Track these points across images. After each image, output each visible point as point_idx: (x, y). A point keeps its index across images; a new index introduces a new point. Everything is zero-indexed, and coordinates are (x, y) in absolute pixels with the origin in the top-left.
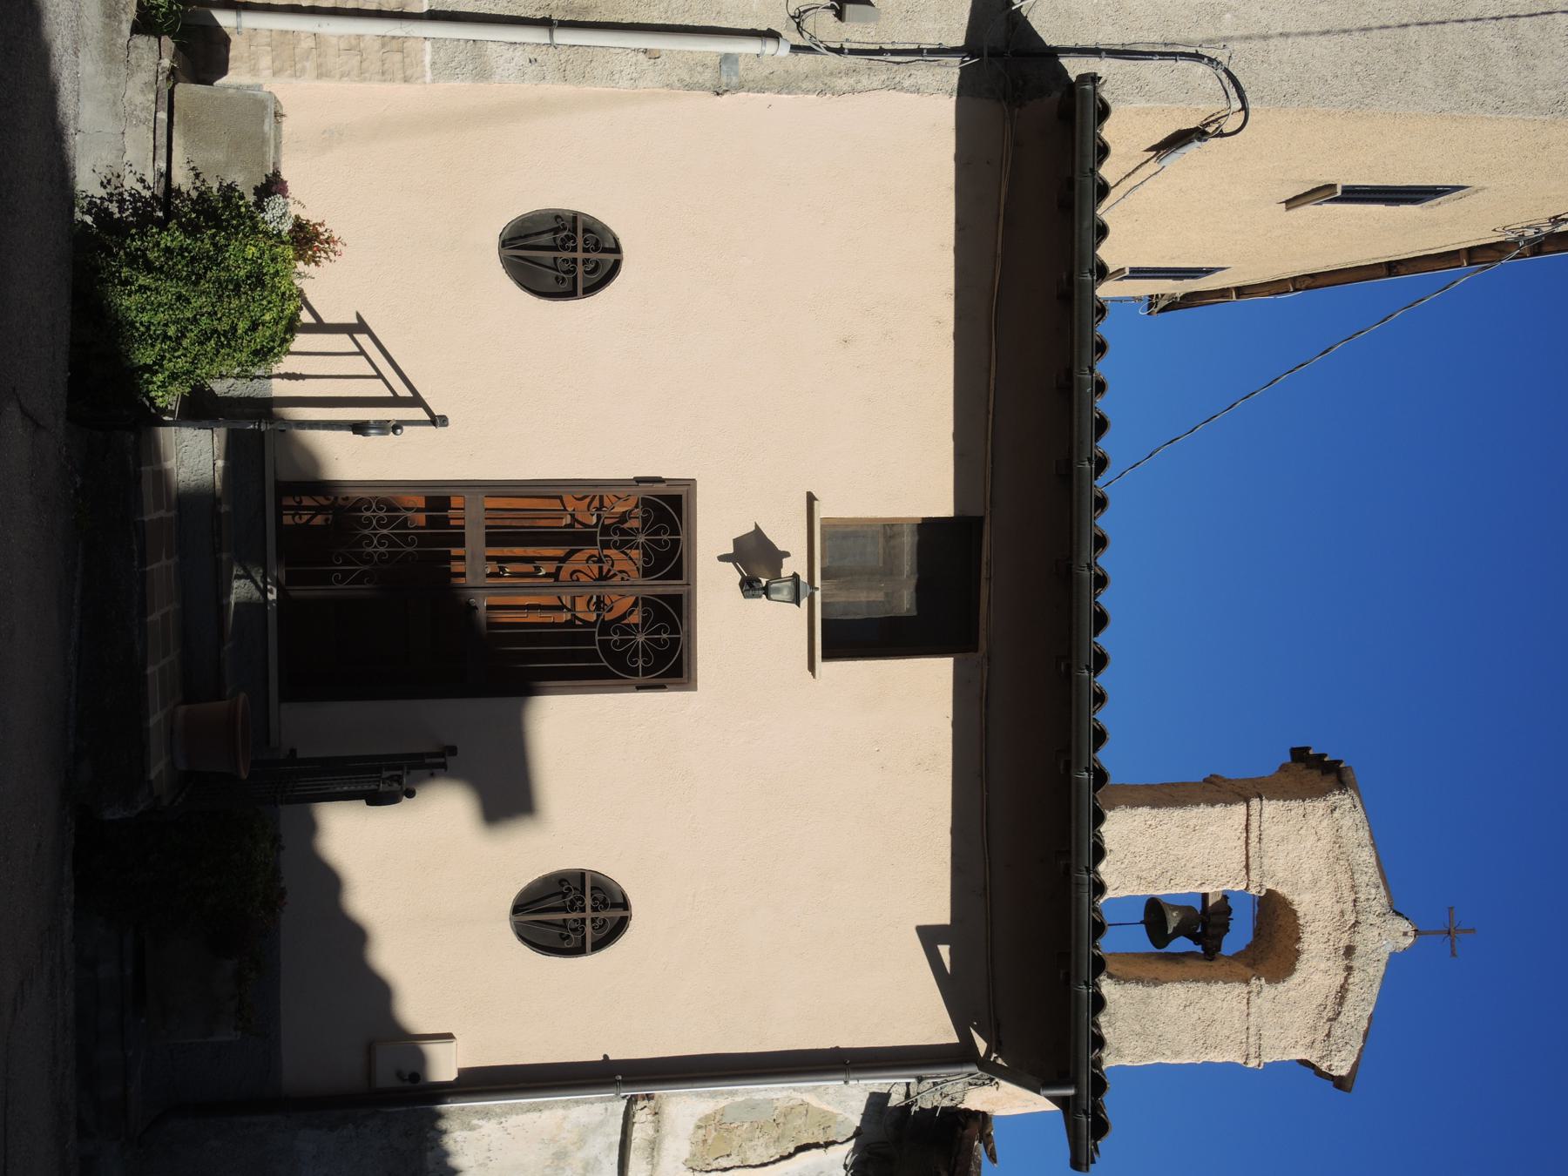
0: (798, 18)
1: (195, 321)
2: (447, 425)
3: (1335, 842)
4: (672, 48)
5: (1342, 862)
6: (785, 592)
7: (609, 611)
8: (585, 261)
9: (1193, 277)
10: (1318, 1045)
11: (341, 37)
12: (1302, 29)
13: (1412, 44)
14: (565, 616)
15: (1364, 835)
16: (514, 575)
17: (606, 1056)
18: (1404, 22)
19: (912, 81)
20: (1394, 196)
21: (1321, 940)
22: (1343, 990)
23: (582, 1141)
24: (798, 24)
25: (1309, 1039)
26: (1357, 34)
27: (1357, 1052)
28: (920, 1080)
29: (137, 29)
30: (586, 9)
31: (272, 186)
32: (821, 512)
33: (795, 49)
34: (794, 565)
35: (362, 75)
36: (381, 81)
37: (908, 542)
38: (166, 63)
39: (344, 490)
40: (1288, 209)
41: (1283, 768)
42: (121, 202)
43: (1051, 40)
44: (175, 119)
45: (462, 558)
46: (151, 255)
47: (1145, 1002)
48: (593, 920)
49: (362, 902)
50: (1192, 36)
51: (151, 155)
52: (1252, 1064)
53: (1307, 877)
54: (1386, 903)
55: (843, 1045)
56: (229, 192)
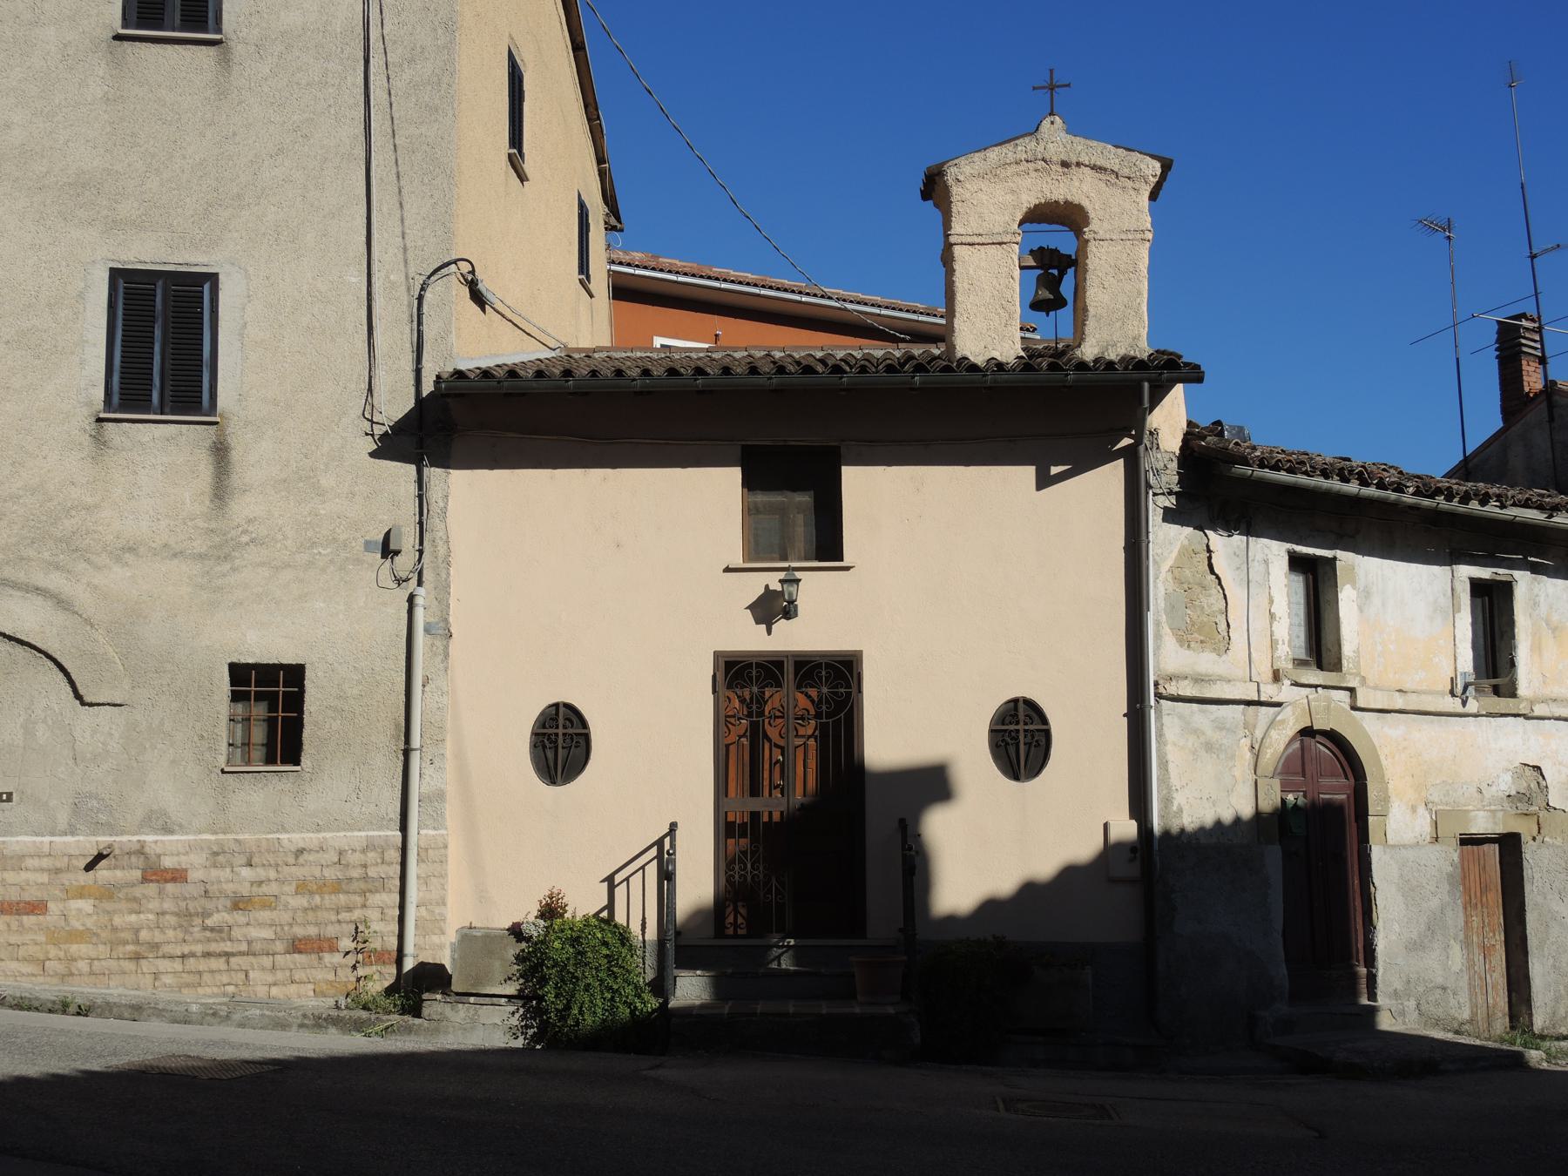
0: (400, 581)
1: (602, 981)
2: (676, 823)
3: (983, 178)
4: (421, 667)
5: (998, 172)
6: (791, 589)
7: (808, 711)
8: (565, 727)
9: (587, 216)
10: (1137, 185)
11: (418, 889)
12: (399, 222)
13: (408, 141)
14: (812, 742)
15: (977, 157)
16: (782, 777)
17: (1124, 715)
18: (392, 147)
19: (440, 501)
20: (517, 94)
21: (1057, 185)
22: (1094, 167)
23: (1196, 732)
24: (403, 581)
25: (1132, 192)
26: (402, 182)
27: (1142, 156)
28: (1149, 486)
29: (418, 1015)
30: (397, 726)
31: (516, 931)
32: (738, 561)
33: (420, 583)
34: (773, 581)
35: (443, 876)
36: (447, 865)
37: (761, 498)
38: (439, 997)
39: (720, 893)
40: (528, 180)
41: (936, 205)
42: (527, 1027)
43: (411, 404)
44: (474, 992)
45: (770, 813)
46: (560, 1007)
47: (1098, 318)
48: (1026, 724)
49: (1004, 884)
50: (406, 303)
51: (497, 1007)
52: (1150, 236)
53: (1009, 197)
54: (1029, 138)
55: (1122, 544)
56: (520, 959)
